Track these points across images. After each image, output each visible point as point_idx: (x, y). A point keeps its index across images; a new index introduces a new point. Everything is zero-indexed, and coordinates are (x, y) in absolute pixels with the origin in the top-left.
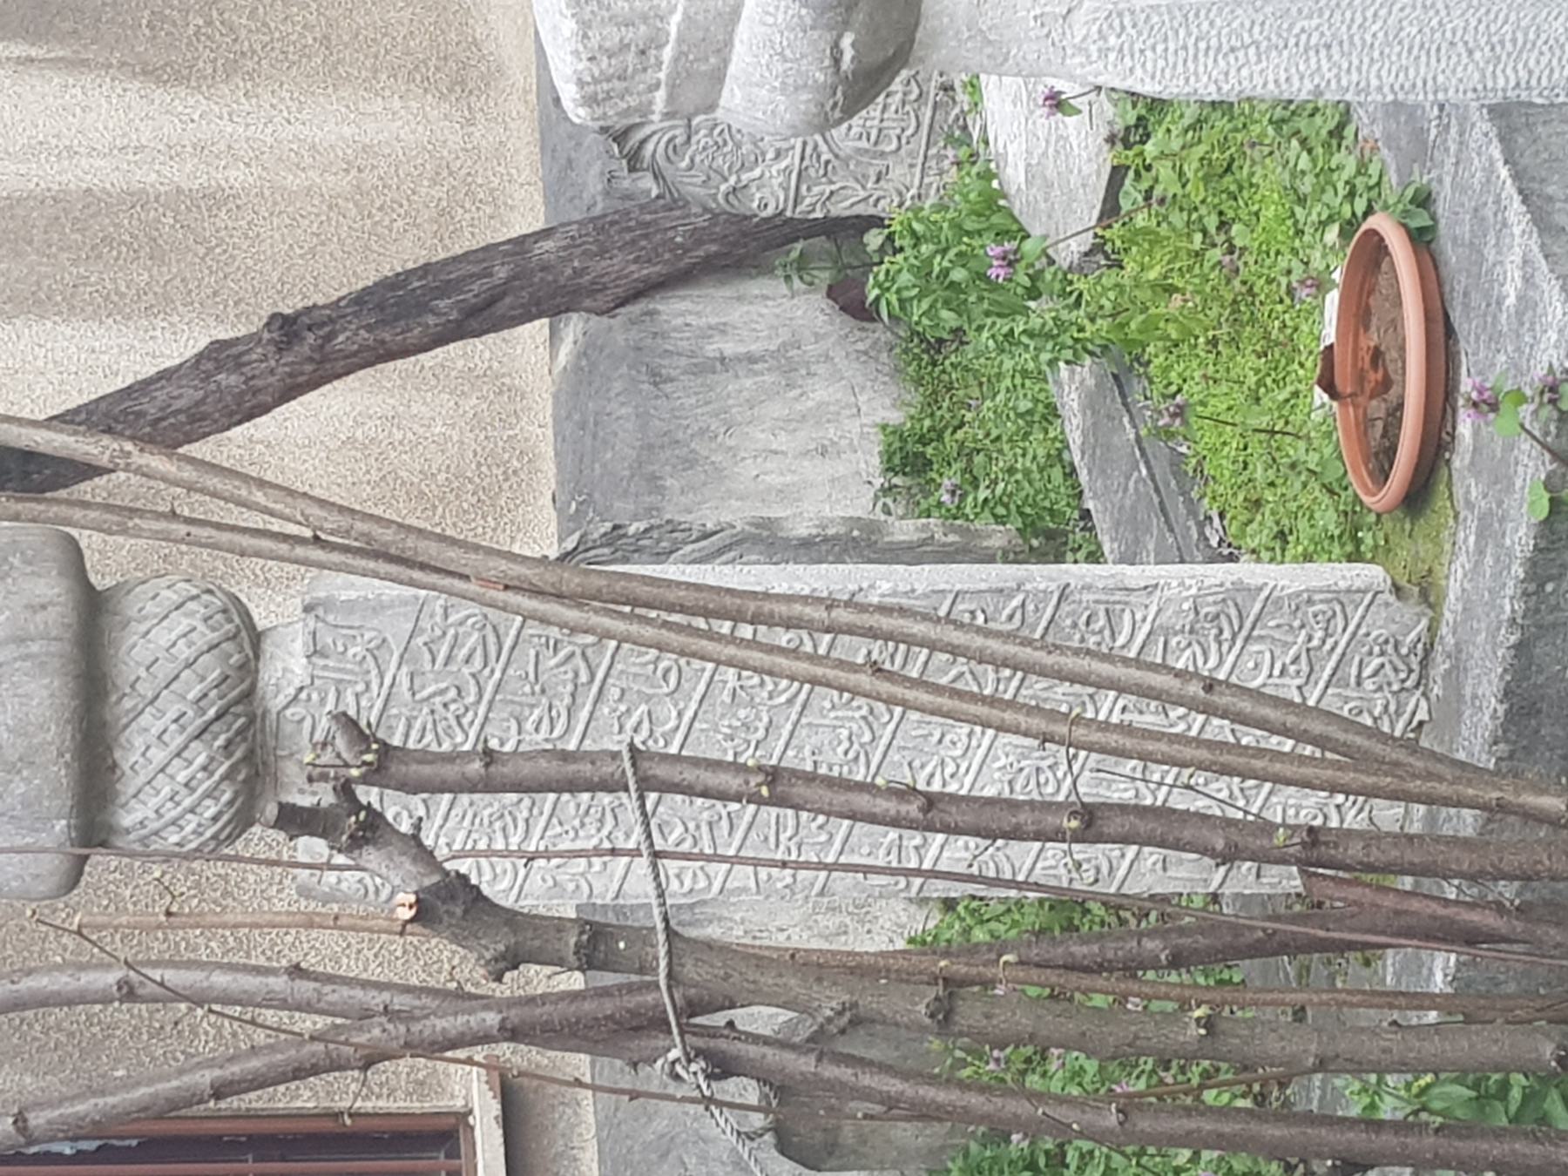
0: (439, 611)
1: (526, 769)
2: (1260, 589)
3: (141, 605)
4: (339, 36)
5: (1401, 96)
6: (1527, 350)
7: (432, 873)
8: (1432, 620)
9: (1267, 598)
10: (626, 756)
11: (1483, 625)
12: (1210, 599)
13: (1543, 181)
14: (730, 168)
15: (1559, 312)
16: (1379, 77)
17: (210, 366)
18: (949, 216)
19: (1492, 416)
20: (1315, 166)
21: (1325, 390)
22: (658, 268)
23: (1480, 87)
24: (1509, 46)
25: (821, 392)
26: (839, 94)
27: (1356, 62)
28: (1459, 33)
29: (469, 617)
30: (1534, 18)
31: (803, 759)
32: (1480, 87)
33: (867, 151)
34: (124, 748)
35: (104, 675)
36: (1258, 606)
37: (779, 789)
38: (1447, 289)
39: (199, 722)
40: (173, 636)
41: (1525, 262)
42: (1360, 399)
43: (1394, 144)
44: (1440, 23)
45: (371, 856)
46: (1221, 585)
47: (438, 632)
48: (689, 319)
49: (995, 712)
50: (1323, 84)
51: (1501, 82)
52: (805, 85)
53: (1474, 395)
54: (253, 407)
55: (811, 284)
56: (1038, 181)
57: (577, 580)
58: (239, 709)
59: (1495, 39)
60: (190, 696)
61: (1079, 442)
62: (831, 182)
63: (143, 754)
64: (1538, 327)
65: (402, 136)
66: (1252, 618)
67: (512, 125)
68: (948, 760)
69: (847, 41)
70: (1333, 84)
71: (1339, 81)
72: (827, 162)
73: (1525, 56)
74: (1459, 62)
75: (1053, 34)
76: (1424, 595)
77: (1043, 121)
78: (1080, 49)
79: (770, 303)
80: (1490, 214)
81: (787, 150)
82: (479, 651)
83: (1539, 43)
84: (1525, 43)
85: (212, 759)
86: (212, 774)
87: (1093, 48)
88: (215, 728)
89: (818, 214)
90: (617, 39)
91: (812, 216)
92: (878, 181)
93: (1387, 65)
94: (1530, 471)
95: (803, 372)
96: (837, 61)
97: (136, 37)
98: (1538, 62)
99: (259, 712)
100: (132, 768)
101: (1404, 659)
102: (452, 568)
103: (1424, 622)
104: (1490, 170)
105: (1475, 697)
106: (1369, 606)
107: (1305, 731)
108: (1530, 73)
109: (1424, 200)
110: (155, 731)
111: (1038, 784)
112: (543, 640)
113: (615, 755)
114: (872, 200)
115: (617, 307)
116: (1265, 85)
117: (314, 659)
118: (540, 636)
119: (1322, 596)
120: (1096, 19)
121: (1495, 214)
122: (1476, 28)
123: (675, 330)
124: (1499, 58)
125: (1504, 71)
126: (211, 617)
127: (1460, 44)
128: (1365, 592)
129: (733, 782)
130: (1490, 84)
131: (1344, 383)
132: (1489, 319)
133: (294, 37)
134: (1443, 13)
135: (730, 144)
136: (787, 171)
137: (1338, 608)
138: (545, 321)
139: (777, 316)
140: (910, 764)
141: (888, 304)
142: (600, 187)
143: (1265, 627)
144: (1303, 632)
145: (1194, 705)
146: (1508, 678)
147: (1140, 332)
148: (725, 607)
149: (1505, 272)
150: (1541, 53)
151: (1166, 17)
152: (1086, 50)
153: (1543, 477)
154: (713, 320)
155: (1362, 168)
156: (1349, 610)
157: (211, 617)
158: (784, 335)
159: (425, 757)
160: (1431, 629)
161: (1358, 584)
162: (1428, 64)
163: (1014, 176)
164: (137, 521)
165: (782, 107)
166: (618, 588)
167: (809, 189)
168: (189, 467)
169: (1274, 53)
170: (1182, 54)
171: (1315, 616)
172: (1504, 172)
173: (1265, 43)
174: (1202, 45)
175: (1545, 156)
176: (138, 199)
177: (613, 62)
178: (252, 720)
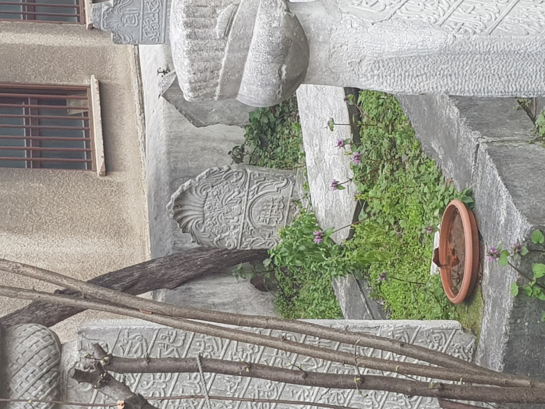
0: (126, 334)
1: (162, 364)
2: (416, 328)
4: (76, 217)
5: (476, 94)
6: (509, 238)
7: (130, 394)
8: (476, 340)
9: (418, 332)
10: (198, 359)
11: (495, 338)
12: (398, 331)
13: (513, 181)
14: (218, 232)
15: (520, 222)
16: (468, 87)
17: (34, 308)
18: (298, 228)
19: (497, 259)
20: (430, 190)
21: (436, 263)
22: (191, 273)
23: (503, 91)
24: (513, 76)
26: (281, 88)
27: (460, 81)
28: (496, 71)
29: (136, 336)
30: (522, 65)
31: (255, 390)
32: (503, 91)
33: (265, 226)
34: (13, 383)
35: (7, 357)
36: (415, 334)
37: (252, 370)
38: (479, 223)
39: (40, 373)
40: (31, 343)
41: (507, 207)
42: (449, 267)
43: (458, 178)
44: (490, 67)
45: (108, 390)
46: (402, 326)
47: (126, 342)
48: (202, 291)
49: (326, 353)
50: (449, 89)
51: (511, 89)
52: (269, 84)
53: (491, 251)
54: (50, 323)
55: (245, 278)
56: (330, 215)
57: (177, 310)
58: (54, 369)
59: (508, 73)
60: (37, 364)
61: (344, 307)
62: (253, 237)
63: (20, 385)
64: (513, 228)
65: (98, 250)
66: (413, 339)
67: (136, 247)
68: (306, 390)
69: (284, 68)
70: (452, 89)
71: (454, 88)
72: (252, 230)
73: (519, 80)
74: (496, 82)
75: (355, 69)
76: (473, 332)
77: (332, 192)
78: (365, 75)
79: (230, 285)
80: (494, 194)
81: (238, 226)
82: (140, 349)
83: (524, 75)
84: (519, 75)
85: (44, 387)
86: (44, 392)
87: (369, 75)
88: (46, 376)
89: (249, 248)
90: (203, 67)
91: (246, 249)
92: (269, 237)
93: (471, 82)
94: (511, 280)
95: (242, 309)
96: (280, 75)
97: (5, 218)
98: (523, 82)
99: (62, 371)
100: (16, 390)
101: (467, 354)
102: (133, 306)
103: (473, 341)
104: (494, 179)
105: (492, 363)
106: (454, 334)
107: (436, 360)
108: (521, 86)
109: (470, 194)
110: (24, 377)
111: (338, 399)
112: (163, 345)
113: (194, 359)
114: (267, 243)
115: (177, 286)
116: (429, 89)
117: (82, 352)
118: (162, 343)
119: (437, 331)
120: (370, 64)
121: (496, 193)
122: (502, 69)
123: (197, 294)
124: (510, 80)
125: (511, 85)
126: (44, 337)
127: (496, 75)
128: (453, 329)
130: (507, 90)
131: (443, 262)
132: (495, 230)
133: (60, 218)
134: (491, 63)
135: (218, 223)
136: (238, 233)
137: (443, 335)
138: (152, 292)
139: (233, 290)
140: (292, 392)
141: (278, 258)
142: (171, 246)
143: (418, 342)
144: (431, 344)
146: (505, 354)
147: (368, 258)
148: (230, 319)
149: (500, 213)
150: (524, 79)
151: (394, 64)
152: (367, 75)
153: (516, 280)
154: (211, 291)
155: (447, 189)
156: (447, 336)
157: (44, 337)
158: (236, 296)
159: (126, 360)
160: (476, 343)
161: (450, 326)
162: (485, 82)
163: (321, 214)
164: (21, 292)
165: (261, 93)
166: (192, 313)
167: (245, 239)
168: (41, 272)
169: (432, 78)
170: (400, 77)
171: (435, 338)
172: (499, 179)
173: (429, 74)
174: (407, 74)
175: (513, 173)
177: (202, 75)
178: (59, 374)
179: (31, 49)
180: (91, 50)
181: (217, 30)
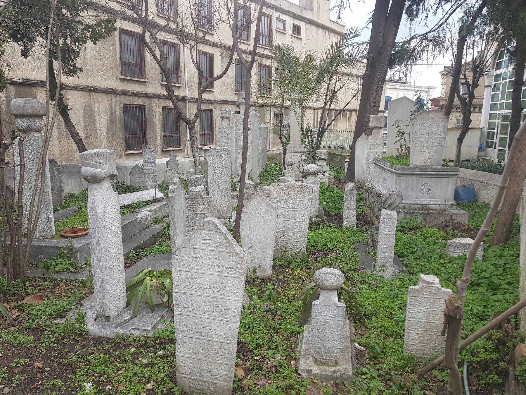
3: (41, 121)
25: (78, 188)
129: (22, 173)
145: (36, 216)
176: (96, 129)
179: (156, 136)
181: (97, 160)
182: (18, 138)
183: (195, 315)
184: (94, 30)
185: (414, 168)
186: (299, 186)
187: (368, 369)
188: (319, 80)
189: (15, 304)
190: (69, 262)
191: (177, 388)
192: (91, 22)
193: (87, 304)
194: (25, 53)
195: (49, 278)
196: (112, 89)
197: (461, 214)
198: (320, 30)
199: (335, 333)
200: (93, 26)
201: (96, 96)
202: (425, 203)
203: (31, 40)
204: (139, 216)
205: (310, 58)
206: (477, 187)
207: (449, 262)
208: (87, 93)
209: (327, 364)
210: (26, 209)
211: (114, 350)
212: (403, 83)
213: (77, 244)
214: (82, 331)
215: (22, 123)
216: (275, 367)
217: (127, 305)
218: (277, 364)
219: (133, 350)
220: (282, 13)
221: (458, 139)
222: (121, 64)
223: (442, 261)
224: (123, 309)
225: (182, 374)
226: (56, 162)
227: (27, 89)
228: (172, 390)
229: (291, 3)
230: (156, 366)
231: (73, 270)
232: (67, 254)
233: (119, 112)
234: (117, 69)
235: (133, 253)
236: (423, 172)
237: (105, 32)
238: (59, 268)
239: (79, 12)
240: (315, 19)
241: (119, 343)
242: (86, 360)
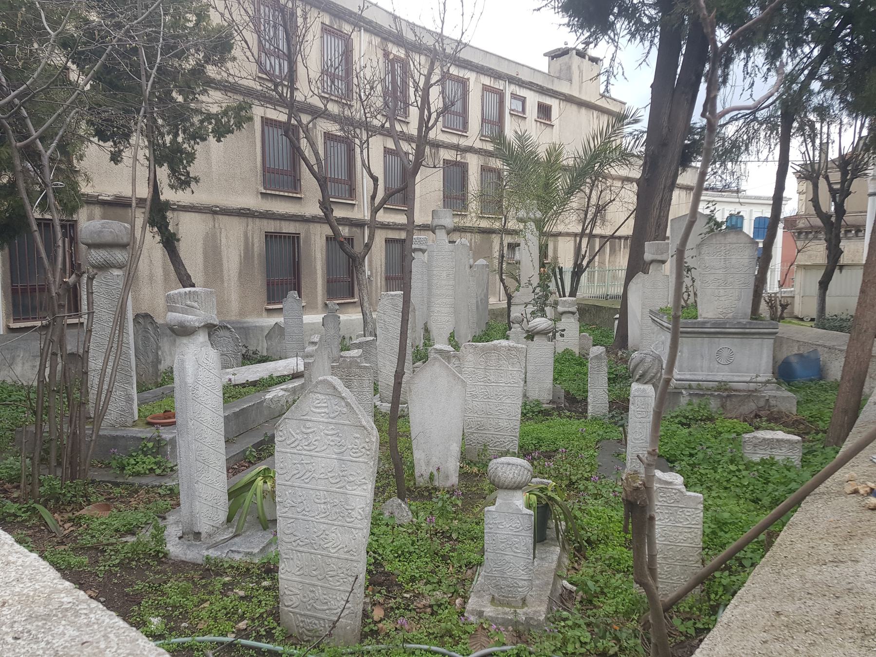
145: (108, 390)
176: (222, 271)
179: (315, 280)
180: (317, 303)
181: (189, 302)
182: (86, 275)
183: (305, 517)
184: (218, 121)
185: (704, 323)
186: (505, 347)
187: (573, 614)
188: (570, 191)
189: (70, 515)
190: (153, 460)
191: (280, 629)
192: (214, 109)
193: (171, 518)
194: (116, 158)
195: (123, 483)
196: (249, 209)
197: (784, 398)
198: (583, 111)
199: (519, 555)
200: (217, 115)
201: (224, 220)
202: (724, 379)
203: (127, 136)
204: (267, 397)
205: (554, 153)
206: (824, 356)
207: (746, 469)
208: (209, 216)
209: (508, 605)
210: (94, 380)
211: (201, 579)
212: (732, 192)
213: (166, 434)
214: (159, 552)
215: (97, 256)
216: (431, 606)
217: (229, 520)
218: (433, 602)
219: (227, 579)
220: (520, 86)
221: (820, 283)
222: (264, 171)
223: (733, 468)
224: (222, 524)
225: (288, 606)
226: (152, 317)
227: (120, 211)
228: (273, 631)
229: (535, 70)
230: (255, 600)
231: (158, 471)
232: (153, 447)
233: (258, 245)
234: (256, 180)
235: (251, 451)
236: (719, 330)
237: (235, 123)
238: (139, 468)
239: (197, 96)
240: (576, 94)
241: (210, 570)
242: (157, 589)
